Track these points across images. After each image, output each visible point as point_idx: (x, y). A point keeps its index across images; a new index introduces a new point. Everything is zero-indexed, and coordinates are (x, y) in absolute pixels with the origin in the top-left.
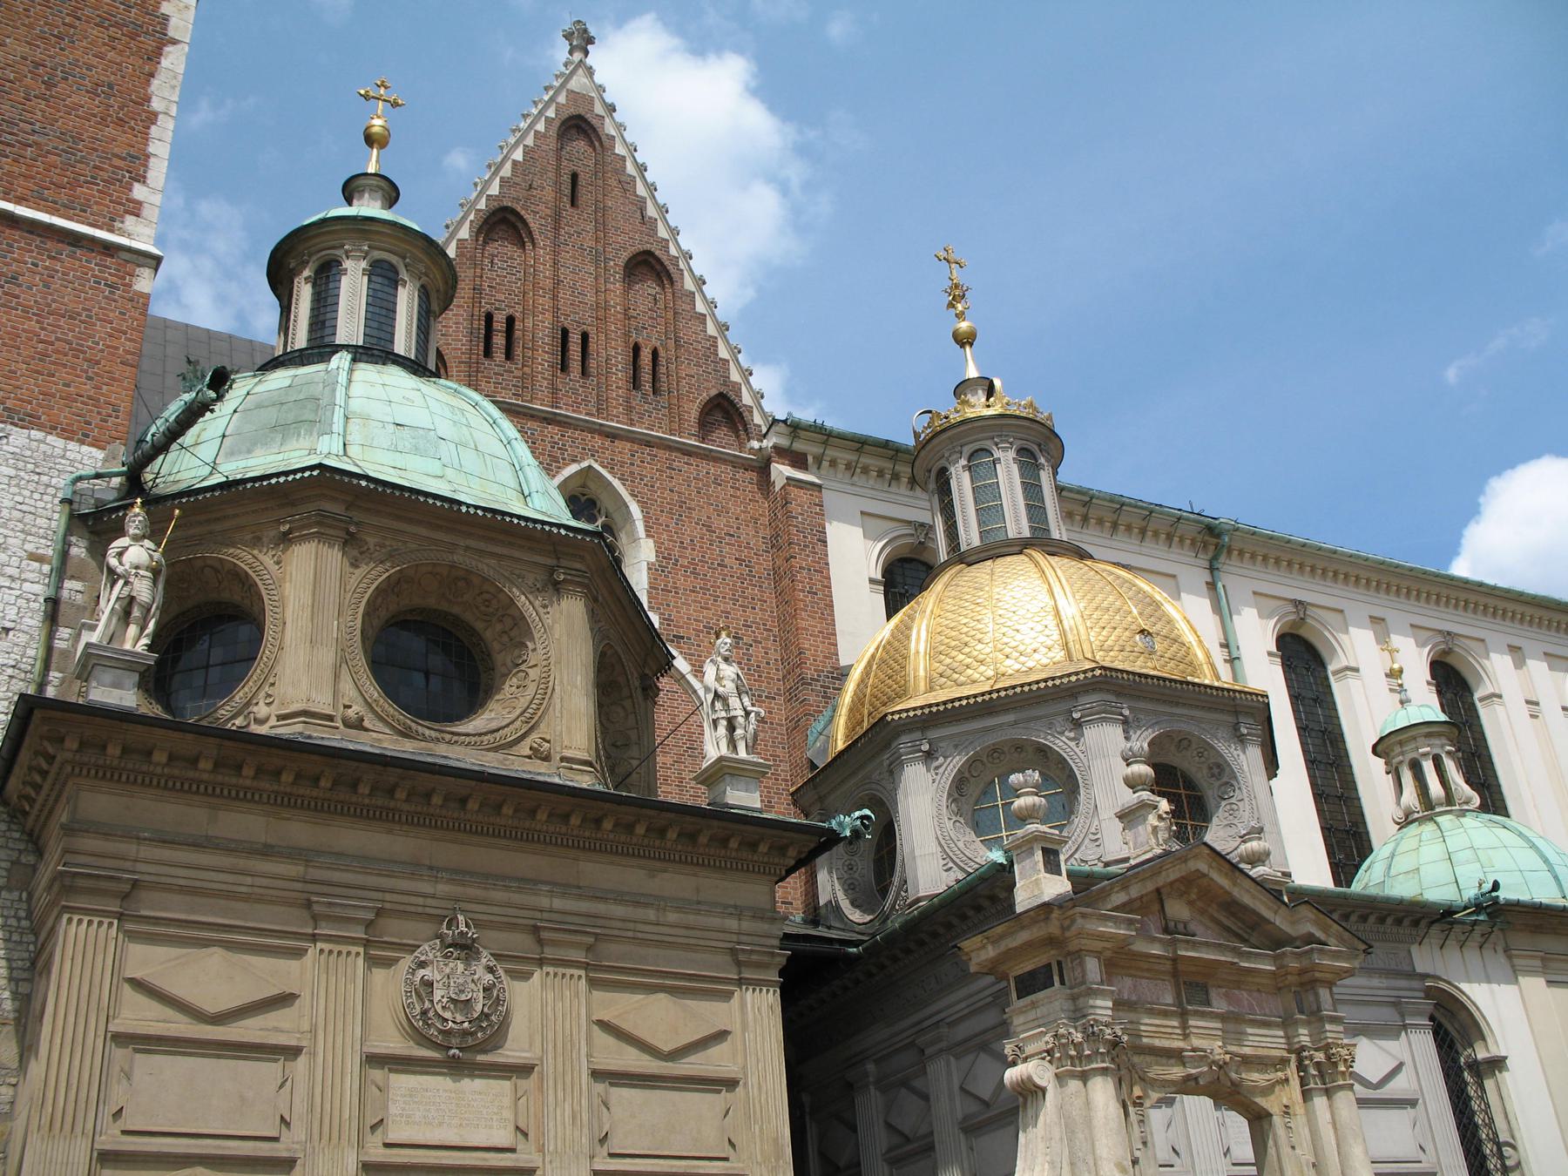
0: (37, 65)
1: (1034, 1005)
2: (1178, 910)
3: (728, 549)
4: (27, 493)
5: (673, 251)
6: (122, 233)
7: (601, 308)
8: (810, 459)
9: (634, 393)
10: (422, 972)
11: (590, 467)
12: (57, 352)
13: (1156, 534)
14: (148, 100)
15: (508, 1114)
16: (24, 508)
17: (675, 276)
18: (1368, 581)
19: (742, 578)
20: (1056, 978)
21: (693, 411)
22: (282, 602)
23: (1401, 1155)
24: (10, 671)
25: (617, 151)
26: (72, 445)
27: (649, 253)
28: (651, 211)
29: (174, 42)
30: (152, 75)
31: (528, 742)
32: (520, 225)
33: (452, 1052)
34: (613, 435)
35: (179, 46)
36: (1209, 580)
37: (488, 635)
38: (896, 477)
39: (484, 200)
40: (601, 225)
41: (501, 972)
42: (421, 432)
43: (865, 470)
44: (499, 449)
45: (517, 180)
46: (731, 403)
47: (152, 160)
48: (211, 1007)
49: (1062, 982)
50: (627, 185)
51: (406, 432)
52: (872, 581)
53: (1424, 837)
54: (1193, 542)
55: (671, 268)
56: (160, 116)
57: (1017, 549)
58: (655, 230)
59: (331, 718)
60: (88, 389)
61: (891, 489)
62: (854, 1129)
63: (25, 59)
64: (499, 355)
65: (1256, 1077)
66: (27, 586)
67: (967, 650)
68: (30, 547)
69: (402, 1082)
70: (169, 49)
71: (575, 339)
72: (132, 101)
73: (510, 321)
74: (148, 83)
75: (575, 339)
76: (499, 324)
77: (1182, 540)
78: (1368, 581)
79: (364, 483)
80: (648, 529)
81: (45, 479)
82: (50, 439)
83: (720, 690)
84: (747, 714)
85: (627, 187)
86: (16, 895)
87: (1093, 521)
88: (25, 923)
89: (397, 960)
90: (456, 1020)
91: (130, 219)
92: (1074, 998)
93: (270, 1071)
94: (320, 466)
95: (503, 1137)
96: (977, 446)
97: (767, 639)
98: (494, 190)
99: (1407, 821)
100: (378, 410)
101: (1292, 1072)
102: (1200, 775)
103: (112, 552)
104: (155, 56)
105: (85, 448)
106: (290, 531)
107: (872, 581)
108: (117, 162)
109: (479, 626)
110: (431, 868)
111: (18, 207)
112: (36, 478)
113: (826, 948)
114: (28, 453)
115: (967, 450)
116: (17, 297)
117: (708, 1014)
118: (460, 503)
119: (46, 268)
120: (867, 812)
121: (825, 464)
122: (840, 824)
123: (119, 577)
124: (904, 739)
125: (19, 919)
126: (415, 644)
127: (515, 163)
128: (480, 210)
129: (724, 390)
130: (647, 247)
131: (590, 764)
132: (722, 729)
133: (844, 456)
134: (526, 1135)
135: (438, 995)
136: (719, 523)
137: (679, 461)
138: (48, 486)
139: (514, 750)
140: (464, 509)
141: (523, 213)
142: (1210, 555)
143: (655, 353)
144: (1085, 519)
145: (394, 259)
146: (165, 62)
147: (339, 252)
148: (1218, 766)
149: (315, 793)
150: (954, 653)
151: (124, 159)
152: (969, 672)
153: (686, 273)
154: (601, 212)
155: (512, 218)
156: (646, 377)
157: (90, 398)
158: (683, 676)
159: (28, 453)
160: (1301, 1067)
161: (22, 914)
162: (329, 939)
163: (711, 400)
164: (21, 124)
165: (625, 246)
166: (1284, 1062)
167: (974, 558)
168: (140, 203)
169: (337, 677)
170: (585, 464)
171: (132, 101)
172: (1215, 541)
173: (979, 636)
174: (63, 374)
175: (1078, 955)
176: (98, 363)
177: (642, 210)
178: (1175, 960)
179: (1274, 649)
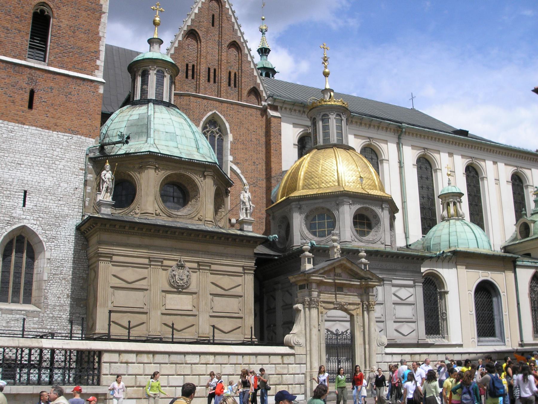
0: (71, 27)
1: (301, 292)
2: (338, 271)
3: (253, 136)
4: (78, 152)
5: (242, 40)
6: (95, 76)
7: (220, 61)
8: (279, 108)
9: (228, 87)
10: (173, 272)
11: (215, 112)
12: (82, 113)
13: (383, 128)
14: (99, 33)
15: (191, 303)
16: (78, 156)
17: (242, 49)
18: (449, 141)
19: (257, 145)
20: (306, 287)
21: (245, 93)
22: (140, 185)
23: (407, 316)
24: (78, 198)
25: (226, 7)
26: (87, 138)
27: (235, 41)
28: (236, 27)
29: (104, 13)
30: (99, 25)
31: (197, 217)
32: (197, 35)
33: (180, 290)
34: (222, 102)
35: (105, 14)
36: (397, 142)
37: (188, 188)
38: (304, 112)
39: (186, 27)
40: (221, 33)
41: (190, 272)
42: (172, 134)
43: (295, 110)
44: (191, 135)
45: (196, 20)
46: (257, 89)
47: (101, 52)
48: (130, 281)
49: (307, 288)
50: (229, 18)
51: (168, 135)
52: (294, 145)
53: (445, 226)
54: (394, 130)
55: (241, 46)
56: (102, 38)
57: (331, 146)
58: (237, 33)
59: (153, 214)
60: (89, 122)
61: (303, 116)
62: (275, 299)
63: (67, 25)
64: (190, 77)
65: (351, 307)
66: (80, 176)
67: (313, 179)
68: (80, 167)
69: (169, 296)
70: (103, 15)
71: (212, 71)
72: (95, 34)
73: (193, 66)
74: (98, 28)
75: (212, 71)
76: (190, 68)
77: (390, 129)
78: (449, 141)
79: (159, 155)
80: (231, 131)
81: (82, 148)
82: (82, 137)
83: (244, 201)
84: (250, 206)
85: (229, 19)
86: (83, 251)
87: (363, 124)
88: (86, 258)
89: (167, 269)
90: (181, 283)
91: (96, 71)
92: (309, 292)
93: (141, 294)
94: (149, 151)
95: (190, 308)
96: (324, 113)
97: (263, 163)
98: (189, 23)
99: (443, 219)
100: (161, 128)
101: (360, 306)
102: (371, 218)
103: (102, 175)
104: (99, 19)
105: (91, 139)
106: (142, 167)
107: (294, 145)
108: (92, 54)
109: (186, 185)
110: (175, 249)
111: (70, 72)
112: (80, 148)
113: (269, 257)
114: (78, 142)
115: (322, 114)
116: (71, 98)
117: (238, 280)
118: (182, 158)
119: (77, 89)
120: (276, 236)
121: (283, 109)
122: (270, 238)
123: (105, 182)
124: (294, 203)
125: (85, 257)
126: (170, 190)
127: (196, 14)
128: (184, 30)
129: (255, 86)
130: (234, 39)
131: (212, 222)
132: (244, 211)
133: (288, 107)
134: (195, 307)
135: (177, 277)
136: (251, 128)
137: (241, 109)
138: (83, 150)
139: (194, 219)
140: (183, 159)
141: (198, 31)
142: (399, 134)
143: (235, 74)
144: (361, 124)
145: (163, 69)
146: (102, 20)
147: (148, 68)
148: (376, 216)
149: (150, 233)
150: (309, 180)
151: (93, 53)
152: (313, 186)
153: (245, 48)
154: (221, 27)
155: (195, 33)
156: (232, 82)
157: (90, 125)
158: (238, 174)
159: (78, 142)
160: (363, 306)
161: (85, 255)
162: (153, 265)
163: (251, 89)
164: (68, 46)
165: (227, 39)
166: (359, 304)
167: (320, 148)
168: (98, 66)
169: (154, 203)
170: (214, 112)
171: (95, 34)
172: (401, 130)
173: (316, 176)
174: (84, 119)
175: (311, 283)
176: (92, 115)
177: (233, 27)
178: (335, 283)
179: (415, 163)
